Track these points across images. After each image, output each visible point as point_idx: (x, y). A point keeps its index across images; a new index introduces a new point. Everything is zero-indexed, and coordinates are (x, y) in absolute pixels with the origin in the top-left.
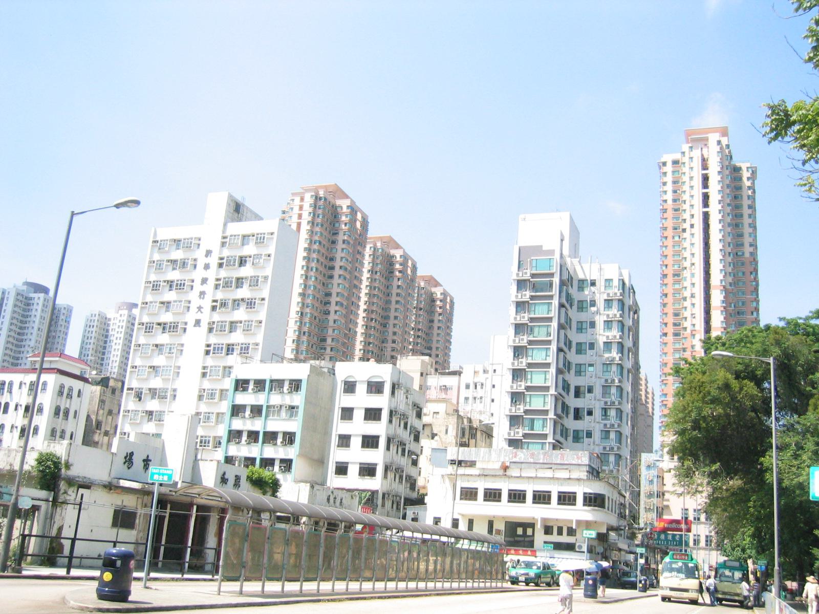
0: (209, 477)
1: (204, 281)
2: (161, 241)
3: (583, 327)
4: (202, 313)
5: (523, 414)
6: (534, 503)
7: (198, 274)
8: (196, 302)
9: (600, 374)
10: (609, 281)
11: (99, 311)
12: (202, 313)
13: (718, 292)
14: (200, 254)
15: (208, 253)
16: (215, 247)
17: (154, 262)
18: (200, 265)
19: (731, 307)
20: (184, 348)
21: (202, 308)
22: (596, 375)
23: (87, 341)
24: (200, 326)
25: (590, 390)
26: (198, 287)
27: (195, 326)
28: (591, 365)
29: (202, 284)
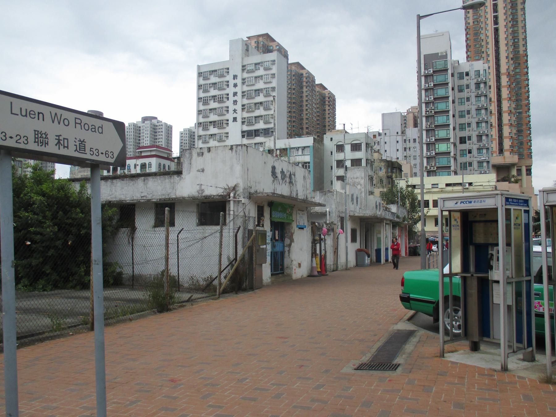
1: (235, 94)
2: (204, 72)
4: (236, 113)
7: (230, 90)
8: (232, 107)
11: (129, 123)
12: (236, 113)
13: (505, 76)
14: (229, 78)
15: (235, 77)
16: (239, 73)
17: (201, 86)
18: (231, 84)
19: (513, 85)
20: (229, 135)
21: (237, 110)
22: (472, 129)
23: (146, 139)
24: (237, 121)
25: (470, 138)
27: (233, 121)
29: (234, 96)
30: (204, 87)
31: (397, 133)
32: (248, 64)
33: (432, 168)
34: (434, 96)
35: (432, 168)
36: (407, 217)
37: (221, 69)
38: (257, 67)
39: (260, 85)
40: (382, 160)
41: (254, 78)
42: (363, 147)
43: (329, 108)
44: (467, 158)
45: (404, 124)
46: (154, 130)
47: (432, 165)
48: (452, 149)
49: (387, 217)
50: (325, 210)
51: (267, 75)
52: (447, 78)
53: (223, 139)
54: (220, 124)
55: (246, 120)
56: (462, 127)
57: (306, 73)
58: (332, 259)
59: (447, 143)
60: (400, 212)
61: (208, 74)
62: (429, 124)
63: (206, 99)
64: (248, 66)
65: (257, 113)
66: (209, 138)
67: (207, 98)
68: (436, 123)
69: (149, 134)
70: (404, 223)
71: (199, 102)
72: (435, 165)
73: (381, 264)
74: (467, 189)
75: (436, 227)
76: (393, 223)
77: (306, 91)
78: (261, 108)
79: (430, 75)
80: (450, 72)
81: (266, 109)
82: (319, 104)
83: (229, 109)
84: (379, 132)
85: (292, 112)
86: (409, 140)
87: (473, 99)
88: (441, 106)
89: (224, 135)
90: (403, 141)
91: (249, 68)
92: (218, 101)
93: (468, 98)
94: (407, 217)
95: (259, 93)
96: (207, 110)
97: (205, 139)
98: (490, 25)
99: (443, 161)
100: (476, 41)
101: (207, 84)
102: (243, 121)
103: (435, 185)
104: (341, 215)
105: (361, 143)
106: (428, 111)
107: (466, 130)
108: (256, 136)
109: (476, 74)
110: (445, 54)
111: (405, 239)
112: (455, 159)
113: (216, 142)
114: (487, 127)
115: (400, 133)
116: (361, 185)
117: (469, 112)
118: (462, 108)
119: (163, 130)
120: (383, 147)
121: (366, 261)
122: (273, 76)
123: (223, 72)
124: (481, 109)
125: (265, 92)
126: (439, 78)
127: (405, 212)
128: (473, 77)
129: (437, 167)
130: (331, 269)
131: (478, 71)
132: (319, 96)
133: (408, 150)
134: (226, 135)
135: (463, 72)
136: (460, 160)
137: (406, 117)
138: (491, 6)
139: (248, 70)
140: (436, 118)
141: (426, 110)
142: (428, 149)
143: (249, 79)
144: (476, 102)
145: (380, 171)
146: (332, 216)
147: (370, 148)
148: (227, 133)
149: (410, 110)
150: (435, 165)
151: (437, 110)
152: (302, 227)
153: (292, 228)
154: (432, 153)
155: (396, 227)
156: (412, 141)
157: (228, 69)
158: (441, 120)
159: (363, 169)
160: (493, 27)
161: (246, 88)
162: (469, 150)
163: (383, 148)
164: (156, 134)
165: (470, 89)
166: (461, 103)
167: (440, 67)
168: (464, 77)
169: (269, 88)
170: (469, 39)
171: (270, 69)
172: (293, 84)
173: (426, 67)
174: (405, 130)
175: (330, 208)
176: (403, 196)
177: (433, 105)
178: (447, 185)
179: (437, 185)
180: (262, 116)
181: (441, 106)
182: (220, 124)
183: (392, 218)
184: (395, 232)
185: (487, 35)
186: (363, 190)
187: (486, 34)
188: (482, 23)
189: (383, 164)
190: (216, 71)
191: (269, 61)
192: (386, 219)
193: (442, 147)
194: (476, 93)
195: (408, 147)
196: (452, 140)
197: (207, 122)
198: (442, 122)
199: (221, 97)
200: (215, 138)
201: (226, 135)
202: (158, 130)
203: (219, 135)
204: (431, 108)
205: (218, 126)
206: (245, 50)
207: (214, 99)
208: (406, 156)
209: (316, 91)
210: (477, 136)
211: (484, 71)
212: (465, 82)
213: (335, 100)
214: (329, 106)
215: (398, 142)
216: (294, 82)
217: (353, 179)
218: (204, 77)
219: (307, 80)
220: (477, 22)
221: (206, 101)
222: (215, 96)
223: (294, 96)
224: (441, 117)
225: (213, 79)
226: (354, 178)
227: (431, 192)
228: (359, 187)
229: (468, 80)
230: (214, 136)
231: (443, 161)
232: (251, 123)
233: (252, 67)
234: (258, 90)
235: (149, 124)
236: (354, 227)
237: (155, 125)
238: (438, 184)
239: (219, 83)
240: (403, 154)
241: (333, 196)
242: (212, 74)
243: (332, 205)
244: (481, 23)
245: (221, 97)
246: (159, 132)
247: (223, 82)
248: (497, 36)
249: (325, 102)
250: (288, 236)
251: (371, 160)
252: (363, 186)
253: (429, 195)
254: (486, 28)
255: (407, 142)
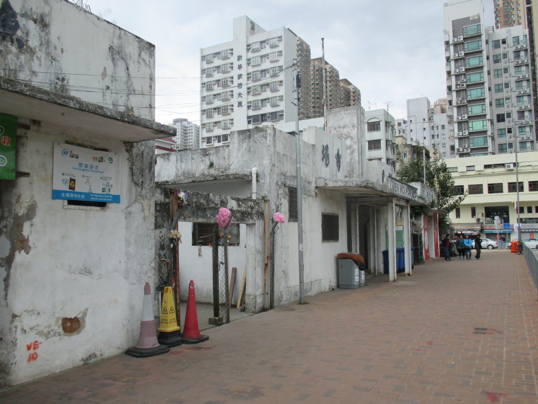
0: (208, 211)
1: (240, 76)
2: (207, 55)
3: (499, 73)
4: (241, 97)
5: (468, 136)
6: (489, 193)
7: (235, 73)
9: (515, 104)
10: (517, 38)
12: (241, 97)
14: (233, 59)
15: (239, 58)
18: (236, 66)
20: (234, 122)
21: (242, 94)
25: (509, 115)
26: (236, 81)
27: (238, 106)
28: (507, 99)
29: (239, 79)
30: (207, 71)
31: (424, 120)
32: (253, 43)
33: (465, 150)
34: (465, 66)
35: (465, 150)
36: (436, 202)
37: (225, 51)
38: (263, 45)
39: (266, 65)
40: (406, 145)
41: (259, 57)
42: (382, 125)
43: (354, 103)
44: (507, 139)
45: (431, 112)
46: (184, 132)
47: (465, 146)
48: (488, 127)
49: (399, 193)
50: (249, 170)
51: (273, 53)
52: (480, 44)
53: (228, 126)
54: (225, 110)
55: (252, 104)
56: (499, 103)
57: (330, 68)
58: (260, 283)
59: (483, 121)
60: (426, 194)
61: (211, 57)
62: (460, 99)
63: (209, 84)
64: (253, 45)
65: (264, 96)
66: (214, 126)
67: (210, 83)
68: (469, 98)
69: (180, 135)
70: (433, 209)
71: (202, 87)
72: (469, 146)
73: (388, 281)
74: (512, 170)
75: (473, 218)
76: (412, 208)
77: (330, 86)
78: (268, 90)
79: (460, 44)
80: (484, 38)
81: (274, 90)
82: (344, 99)
83: (234, 93)
84: (404, 120)
85: (316, 107)
86: (437, 126)
87: (512, 70)
88: (474, 78)
89: (229, 122)
90: (430, 128)
91: (254, 47)
92: (222, 85)
93: (506, 69)
94: (436, 202)
95: (265, 74)
96: (210, 95)
97: (209, 127)
98: (522, 5)
99: (478, 142)
100: (507, 23)
101: (211, 68)
102: (249, 105)
103: (470, 168)
104: (288, 183)
105: (380, 121)
106: (459, 85)
107: (504, 106)
108: (262, 121)
109: (514, 41)
110: (477, 18)
111: (435, 234)
112: (493, 139)
113: (221, 130)
114: (530, 102)
115: (427, 120)
116: (352, 139)
117: (507, 85)
118: (499, 81)
119: (193, 131)
120: (409, 135)
121: (357, 279)
122: (280, 54)
123: (227, 53)
124: (522, 81)
125: (271, 72)
126: (471, 46)
127: (433, 195)
128: (512, 45)
129: (471, 149)
130: (255, 307)
131: (517, 38)
132: (343, 91)
133: (436, 137)
134: (231, 122)
135: (499, 40)
136: (499, 141)
137: (433, 110)
138: (524, 10)
139: (253, 49)
140: (469, 92)
141: (457, 83)
142: (460, 128)
143: (254, 59)
144: (516, 73)
145: (405, 158)
146: (264, 183)
147: (390, 128)
148: (232, 120)
149: (437, 103)
150: (469, 146)
151: (470, 82)
152: (101, 200)
153: (18, 201)
154: (465, 133)
155: (421, 215)
156: (440, 128)
157: (232, 50)
158: (474, 94)
159: (355, 111)
160: (526, 6)
161: (251, 69)
162: (508, 129)
163: (409, 137)
164: (187, 135)
165: (507, 59)
166: (498, 75)
167: (471, 33)
168: (500, 45)
169: (276, 67)
170: (499, 22)
171: (277, 46)
172: (317, 79)
173: (455, 35)
174: (432, 116)
175: (260, 164)
176: (430, 173)
177: (465, 78)
178: (486, 167)
179: (472, 167)
180: (268, 99)
181: (474, 78)
182: (225, 110)
183: (410, 197)
184: (419, 222)
185: (519, 16)
186: (356, 147)
187: (518, 15)
188: (513, 4)
189: (407, 149)
190: (219, 53)
191: (275, 38)
192: (400, 198)
193: (477, 125)
194: (516, 62)
195: (436, 134)
196: (488, 117)
197: (211, 109)
198: (476, 97)
199: (225, 81)
200: (219, 125)
201: (231, 122)
202: (188, 131)
203: (224, 122)
204: (463, 80)
205: (222, 113)
206: (250, 28)
207: (218, 84)
208: (434, 144)
209: (341, 86)
210: (518, 112)
211: (525, 36)
212: (501, 50)
213: (360, 95)
214: (354, 101)
215: (424, 129)
216: (317, 78)
217: (338, 129)
218: (207, 61)
219: (330, 75)
220: (507, 4)
221: (209, 86)
222: (219, 81)
223: (318, 91)
224: (474, 90)
225: (217, 62)
226: (339, 128)
227: (466, 175)
228: (348, 142)
229: (505, 48)
230: (219, 123)
231: (478, 142)
232: (257, 107)
233: (258, 46)
234: (265, 70)
235: (180, 126)
236: (331, 210)
237: (185, 127)
238: (474, 166)
239: (222, 65)
240: (430, 132)
241: (266, 138)
242: (216, 57)
243: (263, 158)
244: (512, 4)
245: (225, 81)
246: (189, 133)
247: (227, 64)
248: (530, 17)
249: (349, 97)
250: (6, 227)
251: (391, 141)
252: (356, 140)
253: (463, 179)
254: (518, 9)
255: (435, 129)
